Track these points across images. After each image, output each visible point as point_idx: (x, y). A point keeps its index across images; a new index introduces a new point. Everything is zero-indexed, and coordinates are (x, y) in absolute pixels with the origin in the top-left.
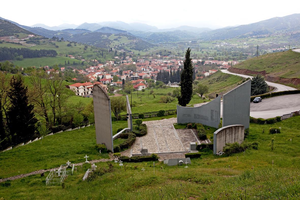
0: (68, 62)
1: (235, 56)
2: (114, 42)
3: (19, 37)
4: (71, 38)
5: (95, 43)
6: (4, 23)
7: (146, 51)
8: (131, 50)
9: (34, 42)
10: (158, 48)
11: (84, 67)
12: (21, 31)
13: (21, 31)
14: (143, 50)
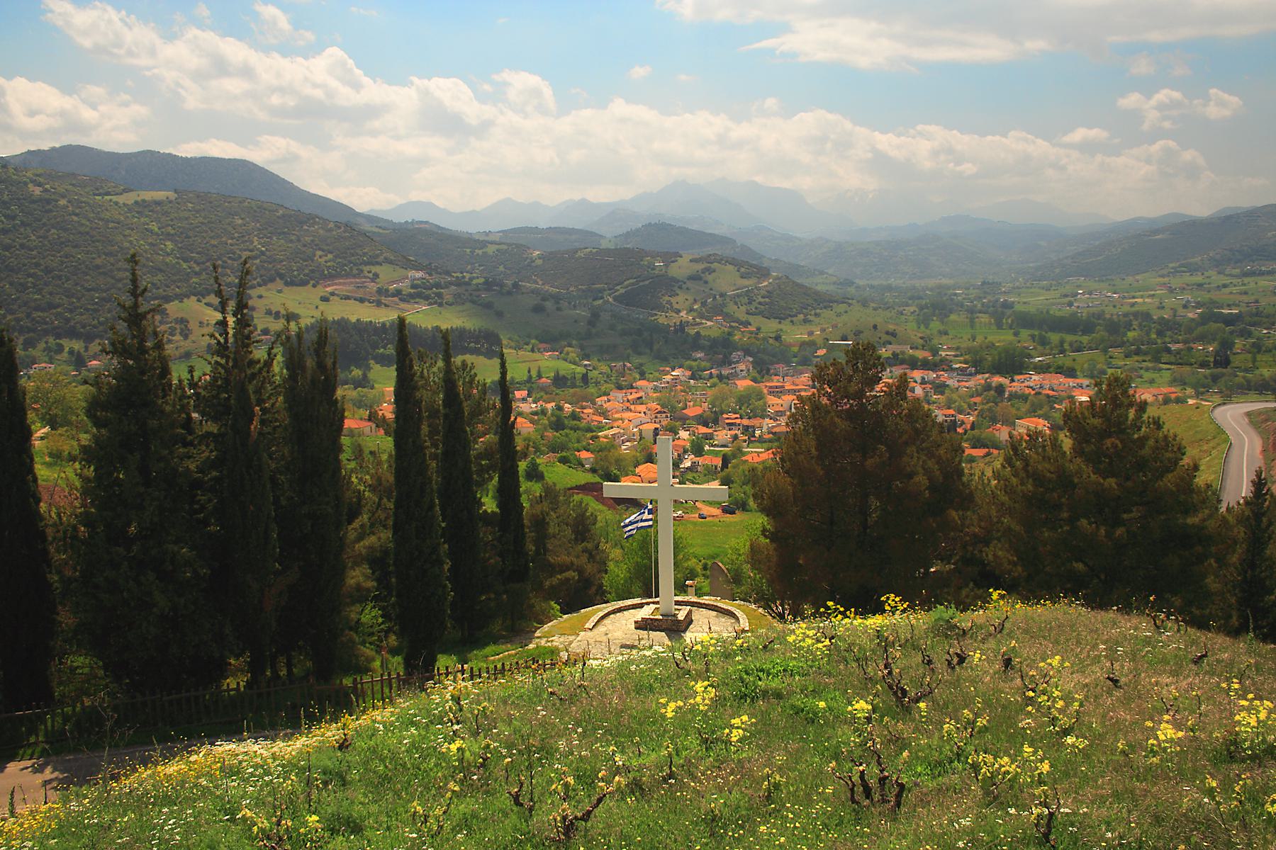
0: (539, 372)
1: (1135, 354)
2: (688, 289)
3: (378, 280)
4: (533, 264)
5: (618, 287)
6: (334, 233)
7: (806, 321)
8: (751, 319)
9: (427, 298)
10: (848, 309)
11: (592, 390)
12: (385, 258)
13: (385, 258)
14: (794, 319)
